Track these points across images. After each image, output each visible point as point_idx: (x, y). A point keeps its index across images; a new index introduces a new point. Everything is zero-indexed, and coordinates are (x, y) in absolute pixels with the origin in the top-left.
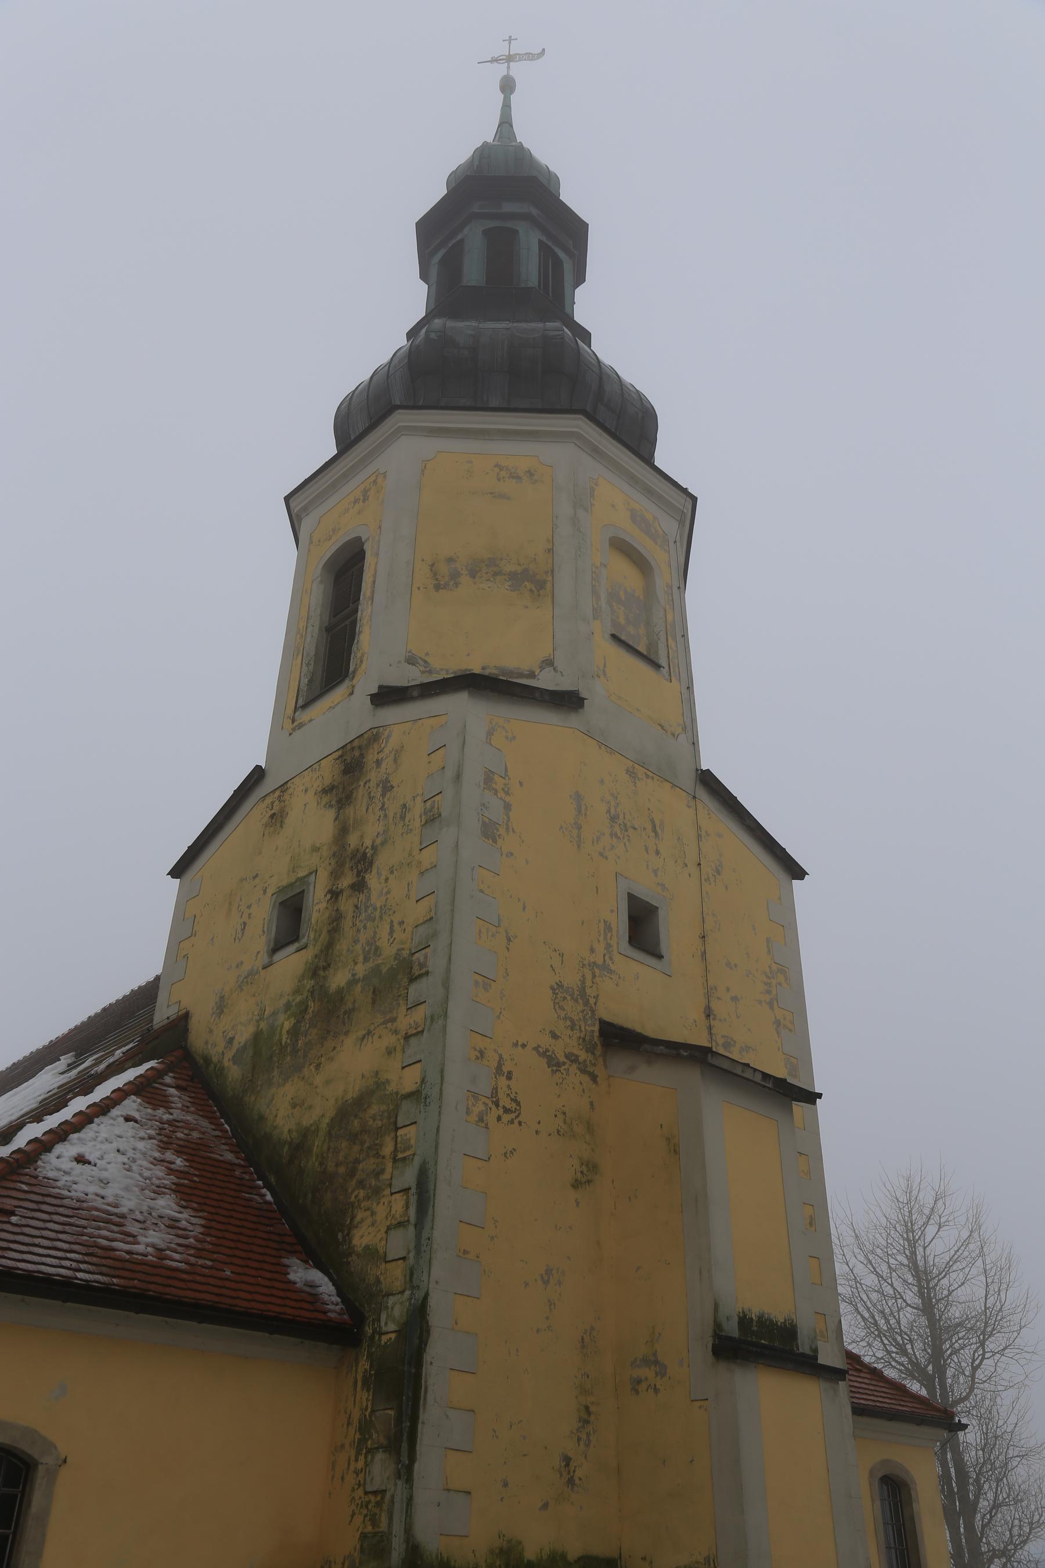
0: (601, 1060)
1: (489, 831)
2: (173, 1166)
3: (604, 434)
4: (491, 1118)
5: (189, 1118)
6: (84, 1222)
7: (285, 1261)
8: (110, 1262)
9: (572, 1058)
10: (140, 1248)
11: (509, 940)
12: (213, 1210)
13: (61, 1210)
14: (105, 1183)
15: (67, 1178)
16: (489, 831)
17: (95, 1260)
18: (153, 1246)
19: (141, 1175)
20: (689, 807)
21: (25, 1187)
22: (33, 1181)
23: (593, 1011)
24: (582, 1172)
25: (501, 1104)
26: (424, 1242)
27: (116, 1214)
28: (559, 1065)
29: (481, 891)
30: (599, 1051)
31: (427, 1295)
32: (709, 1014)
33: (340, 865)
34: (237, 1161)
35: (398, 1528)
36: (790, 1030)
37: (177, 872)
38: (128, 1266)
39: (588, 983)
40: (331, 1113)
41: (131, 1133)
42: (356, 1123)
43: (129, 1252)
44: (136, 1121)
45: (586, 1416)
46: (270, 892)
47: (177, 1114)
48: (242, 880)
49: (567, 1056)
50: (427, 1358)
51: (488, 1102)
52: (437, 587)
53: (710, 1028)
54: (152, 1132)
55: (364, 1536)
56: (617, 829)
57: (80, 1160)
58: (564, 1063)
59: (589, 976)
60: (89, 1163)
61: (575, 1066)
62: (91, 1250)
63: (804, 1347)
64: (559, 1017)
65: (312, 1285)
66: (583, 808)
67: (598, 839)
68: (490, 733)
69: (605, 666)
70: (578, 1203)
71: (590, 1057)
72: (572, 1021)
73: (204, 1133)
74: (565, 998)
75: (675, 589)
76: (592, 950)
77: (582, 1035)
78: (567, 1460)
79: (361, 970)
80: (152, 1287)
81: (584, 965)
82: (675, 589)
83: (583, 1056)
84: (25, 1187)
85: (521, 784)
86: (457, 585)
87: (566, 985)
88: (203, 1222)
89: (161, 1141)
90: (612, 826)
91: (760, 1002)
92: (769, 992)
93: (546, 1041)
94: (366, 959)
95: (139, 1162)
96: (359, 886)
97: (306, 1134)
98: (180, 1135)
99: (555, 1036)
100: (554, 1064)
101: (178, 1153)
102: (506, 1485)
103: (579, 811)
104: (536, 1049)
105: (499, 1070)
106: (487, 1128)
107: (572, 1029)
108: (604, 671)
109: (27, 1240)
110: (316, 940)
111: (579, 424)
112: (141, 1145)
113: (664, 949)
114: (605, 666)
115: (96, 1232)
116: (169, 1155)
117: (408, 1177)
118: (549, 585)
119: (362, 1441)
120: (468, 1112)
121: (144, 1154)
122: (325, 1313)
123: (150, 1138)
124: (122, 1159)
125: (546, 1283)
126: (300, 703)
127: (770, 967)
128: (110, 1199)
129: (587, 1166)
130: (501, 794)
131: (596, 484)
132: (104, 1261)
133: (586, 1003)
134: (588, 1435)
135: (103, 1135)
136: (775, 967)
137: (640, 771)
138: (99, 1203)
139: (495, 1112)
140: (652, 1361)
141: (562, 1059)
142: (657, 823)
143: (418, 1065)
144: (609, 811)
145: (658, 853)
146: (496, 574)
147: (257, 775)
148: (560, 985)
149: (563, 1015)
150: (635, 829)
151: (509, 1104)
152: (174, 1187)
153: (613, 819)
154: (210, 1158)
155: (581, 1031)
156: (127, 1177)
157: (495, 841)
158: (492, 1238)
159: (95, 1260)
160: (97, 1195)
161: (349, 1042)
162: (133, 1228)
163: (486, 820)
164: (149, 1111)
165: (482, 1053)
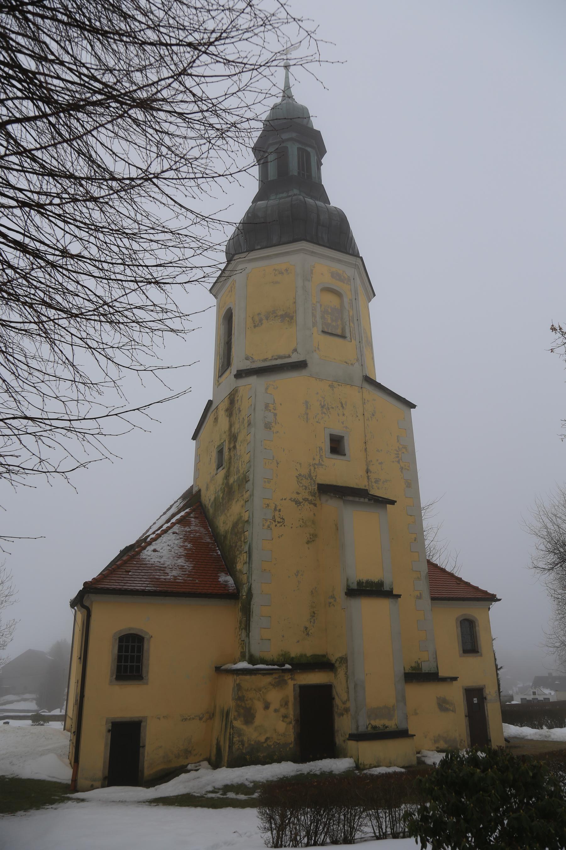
0: (318, 498)
1: (268, 426)
2: (187, 547)
3: (315, 245)
4: (273, 526)
5: (197, 528)
6: (152, 571)
7: (219, 575)
8: (158, 583)
9: (306, 500)
10: (169, 577)
11: (278, 463)
12: (197, 560)
13: (146, 568)
14: (161, 557)
15: (149, 558)
16: (268, 426)
17: (153, 583)
18: (173, 576)
19: (174, 552)
20: (359, 392)
21: (135, 563)
22: (138, 560)
23: (314, 481)
24: (310, 538)
25: (276, 520)
26: (250, 568)
27: (163, 567)
28: (300, 503)
29: (266, 449)
30: (317, 495)
31: (251, 584)
32: (368, 471)
33: (230, 439)
34: (211, 542)
35: (247, 650)
36: (408, 470)
37: (194, 438)
38: (164, 583)
39: (312, 471)
40: (231, 526)
41: (174, 538)
42: (236, 530)
43: (165, 579)
44: (177, 533)
45: (313, 615)
46: (216, 447)
47: (192, 528)
48: (210, 442)
49: (303, 500)
50: (252, 603)
51: (272, 521)
52: (255, 327)
53: (368, 477)
54: (181, 536)
55: (241, 652)
56: (324, 410)
57: (155, 551)
58: (302, 502)
59: (312, 469)
60: (157, 551)
61: (307, 502)
62: (152, 580)
63: (386, 588)
64: (300, 486)
65: (226, 582)
66: (309, 406)
67: (316, 416)
68: (267, 389)
69: (318, 345)
70: (309, 549)
71: (313, 498)
72: (305, 486)
73: (201, 533)
74: (302, 479)
75: (354, 300)
76: (314, 459)
77: (310, 491)
78: (306, 628)
79: (236, 477)
80: (169, 589)
81: (310, 465)
82: (354, 300)
83: (310, 498)
84: (135, 563)
85: (281, 404)
86: (262, 324)
87: (302, 474)
88: (192, 565)
89: (184, 539)
90: (322, 410)
91: (393, 462)
92: (398, 457)
93: (295, 496)
94: (237, 474)
95: (175, 548)
96: (235, 447)
97: (226, 532)
98: (192, 535)
99: (298, 493)
100: (297, 503)
101: (190, 542)
102: (283, 636)
103: (307, 408)
104: (290, 499)
105: (275, 509)
106: (271, 529)
107: (306, 489)
108: (318, 348)
109: (133, 579)
110: (226, 466)
111: (304, 245)
112: (176, 542)
113: (347, 451)
114: (318, 345)
115: (155, 574)
116: (186, 544)
117: (246, 549)
118: (294, 318)
119: (240, 626)
120: (263, 525)
121: (177, 545)
122: (228, 590)
123: (181, 538)
124: (169, 548)
125: (297, 576)
126: (220, 375)
127: (398, 447)
128: (162, 563)
129: (313, 535)
130: (272, 411)
131: (314, 267)
132: (156, 583)
133: (312, 479)
134: (314, 620)
135: (164, 540)
136: (401, 447)
137: (335, 384)
138: (158, 564)
139: (274, 524)
140: (333, 597)
141: (301, 500)
142: (343, 403)
143: (248, 512)
144: (321, 404)
145: (344, 415)
146: (275, 317)
147: (210, 403)
148: (300, 475)
149: (301, 485)
150: (333, 408)
151: (279, 520)
152: (185, 555)
153: (323, 407)
154: (201, 542)
155: (309, 489)
156: (169, 554)
157: (270, 429)
158: (275, 564)
159: (153, 583)
160: (158, 562)
161: (234, 502)
162: (168, 571)
163: (267, 422)
164: (183, 528)
165: (268, 505)
